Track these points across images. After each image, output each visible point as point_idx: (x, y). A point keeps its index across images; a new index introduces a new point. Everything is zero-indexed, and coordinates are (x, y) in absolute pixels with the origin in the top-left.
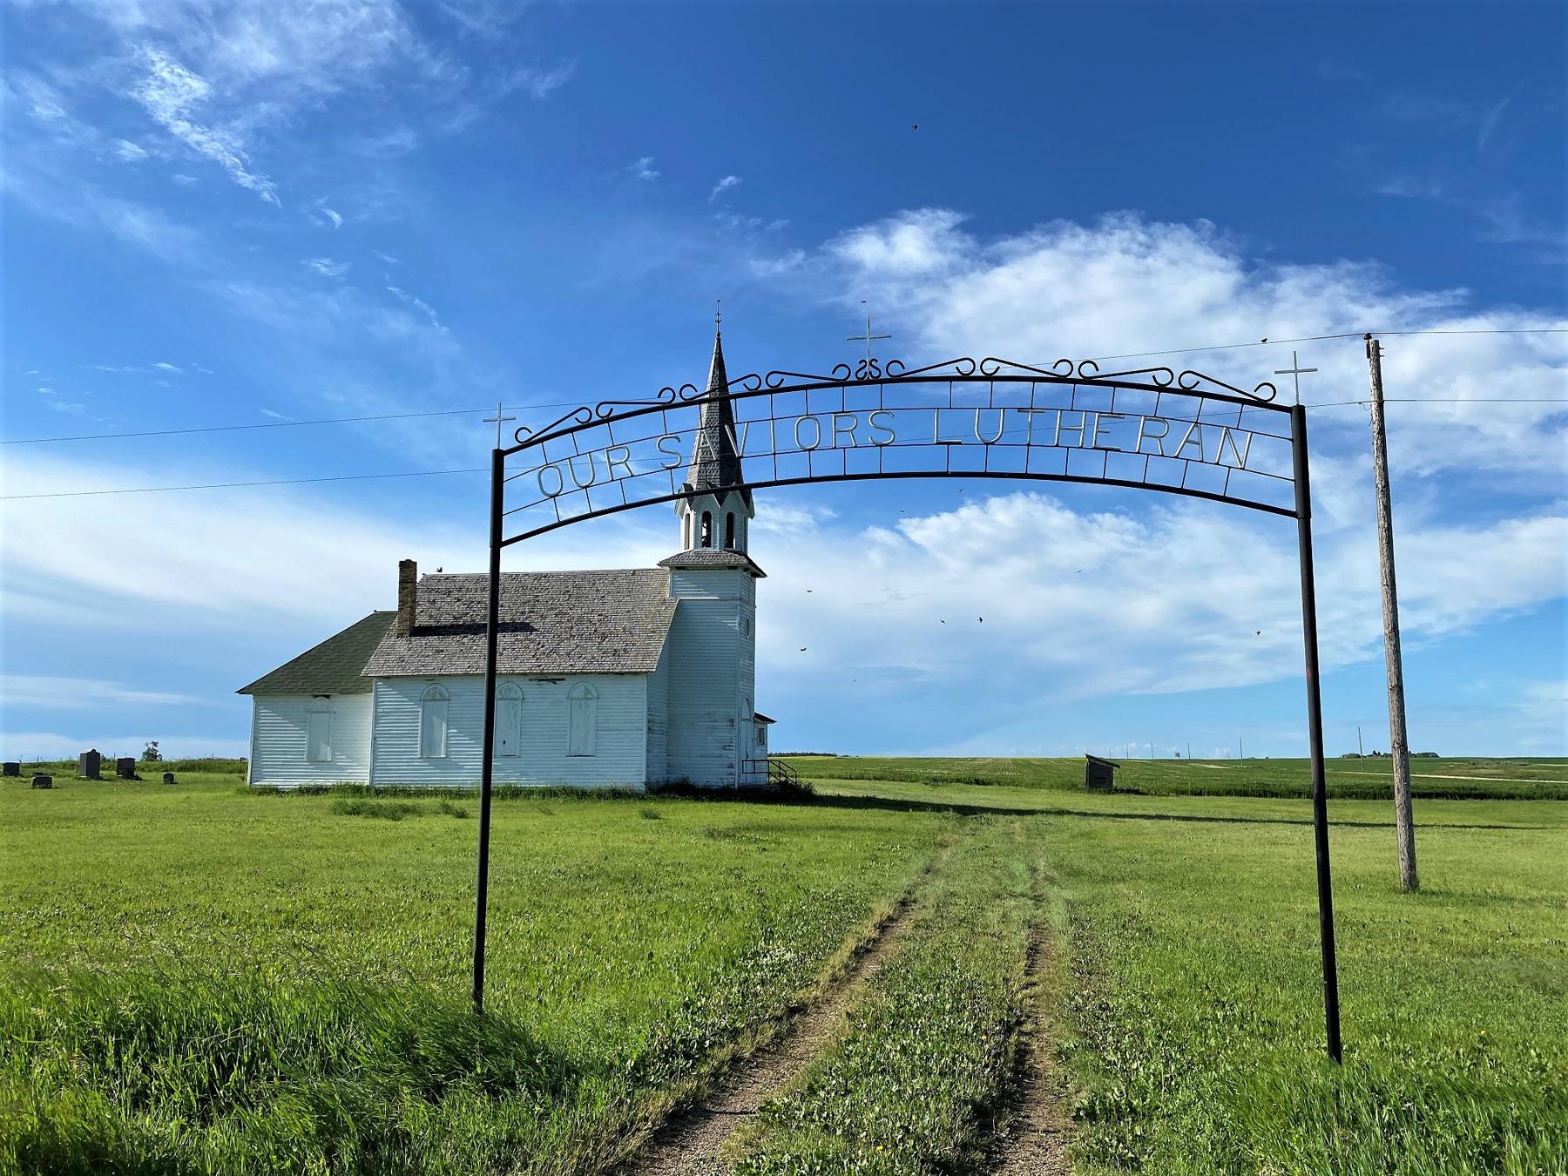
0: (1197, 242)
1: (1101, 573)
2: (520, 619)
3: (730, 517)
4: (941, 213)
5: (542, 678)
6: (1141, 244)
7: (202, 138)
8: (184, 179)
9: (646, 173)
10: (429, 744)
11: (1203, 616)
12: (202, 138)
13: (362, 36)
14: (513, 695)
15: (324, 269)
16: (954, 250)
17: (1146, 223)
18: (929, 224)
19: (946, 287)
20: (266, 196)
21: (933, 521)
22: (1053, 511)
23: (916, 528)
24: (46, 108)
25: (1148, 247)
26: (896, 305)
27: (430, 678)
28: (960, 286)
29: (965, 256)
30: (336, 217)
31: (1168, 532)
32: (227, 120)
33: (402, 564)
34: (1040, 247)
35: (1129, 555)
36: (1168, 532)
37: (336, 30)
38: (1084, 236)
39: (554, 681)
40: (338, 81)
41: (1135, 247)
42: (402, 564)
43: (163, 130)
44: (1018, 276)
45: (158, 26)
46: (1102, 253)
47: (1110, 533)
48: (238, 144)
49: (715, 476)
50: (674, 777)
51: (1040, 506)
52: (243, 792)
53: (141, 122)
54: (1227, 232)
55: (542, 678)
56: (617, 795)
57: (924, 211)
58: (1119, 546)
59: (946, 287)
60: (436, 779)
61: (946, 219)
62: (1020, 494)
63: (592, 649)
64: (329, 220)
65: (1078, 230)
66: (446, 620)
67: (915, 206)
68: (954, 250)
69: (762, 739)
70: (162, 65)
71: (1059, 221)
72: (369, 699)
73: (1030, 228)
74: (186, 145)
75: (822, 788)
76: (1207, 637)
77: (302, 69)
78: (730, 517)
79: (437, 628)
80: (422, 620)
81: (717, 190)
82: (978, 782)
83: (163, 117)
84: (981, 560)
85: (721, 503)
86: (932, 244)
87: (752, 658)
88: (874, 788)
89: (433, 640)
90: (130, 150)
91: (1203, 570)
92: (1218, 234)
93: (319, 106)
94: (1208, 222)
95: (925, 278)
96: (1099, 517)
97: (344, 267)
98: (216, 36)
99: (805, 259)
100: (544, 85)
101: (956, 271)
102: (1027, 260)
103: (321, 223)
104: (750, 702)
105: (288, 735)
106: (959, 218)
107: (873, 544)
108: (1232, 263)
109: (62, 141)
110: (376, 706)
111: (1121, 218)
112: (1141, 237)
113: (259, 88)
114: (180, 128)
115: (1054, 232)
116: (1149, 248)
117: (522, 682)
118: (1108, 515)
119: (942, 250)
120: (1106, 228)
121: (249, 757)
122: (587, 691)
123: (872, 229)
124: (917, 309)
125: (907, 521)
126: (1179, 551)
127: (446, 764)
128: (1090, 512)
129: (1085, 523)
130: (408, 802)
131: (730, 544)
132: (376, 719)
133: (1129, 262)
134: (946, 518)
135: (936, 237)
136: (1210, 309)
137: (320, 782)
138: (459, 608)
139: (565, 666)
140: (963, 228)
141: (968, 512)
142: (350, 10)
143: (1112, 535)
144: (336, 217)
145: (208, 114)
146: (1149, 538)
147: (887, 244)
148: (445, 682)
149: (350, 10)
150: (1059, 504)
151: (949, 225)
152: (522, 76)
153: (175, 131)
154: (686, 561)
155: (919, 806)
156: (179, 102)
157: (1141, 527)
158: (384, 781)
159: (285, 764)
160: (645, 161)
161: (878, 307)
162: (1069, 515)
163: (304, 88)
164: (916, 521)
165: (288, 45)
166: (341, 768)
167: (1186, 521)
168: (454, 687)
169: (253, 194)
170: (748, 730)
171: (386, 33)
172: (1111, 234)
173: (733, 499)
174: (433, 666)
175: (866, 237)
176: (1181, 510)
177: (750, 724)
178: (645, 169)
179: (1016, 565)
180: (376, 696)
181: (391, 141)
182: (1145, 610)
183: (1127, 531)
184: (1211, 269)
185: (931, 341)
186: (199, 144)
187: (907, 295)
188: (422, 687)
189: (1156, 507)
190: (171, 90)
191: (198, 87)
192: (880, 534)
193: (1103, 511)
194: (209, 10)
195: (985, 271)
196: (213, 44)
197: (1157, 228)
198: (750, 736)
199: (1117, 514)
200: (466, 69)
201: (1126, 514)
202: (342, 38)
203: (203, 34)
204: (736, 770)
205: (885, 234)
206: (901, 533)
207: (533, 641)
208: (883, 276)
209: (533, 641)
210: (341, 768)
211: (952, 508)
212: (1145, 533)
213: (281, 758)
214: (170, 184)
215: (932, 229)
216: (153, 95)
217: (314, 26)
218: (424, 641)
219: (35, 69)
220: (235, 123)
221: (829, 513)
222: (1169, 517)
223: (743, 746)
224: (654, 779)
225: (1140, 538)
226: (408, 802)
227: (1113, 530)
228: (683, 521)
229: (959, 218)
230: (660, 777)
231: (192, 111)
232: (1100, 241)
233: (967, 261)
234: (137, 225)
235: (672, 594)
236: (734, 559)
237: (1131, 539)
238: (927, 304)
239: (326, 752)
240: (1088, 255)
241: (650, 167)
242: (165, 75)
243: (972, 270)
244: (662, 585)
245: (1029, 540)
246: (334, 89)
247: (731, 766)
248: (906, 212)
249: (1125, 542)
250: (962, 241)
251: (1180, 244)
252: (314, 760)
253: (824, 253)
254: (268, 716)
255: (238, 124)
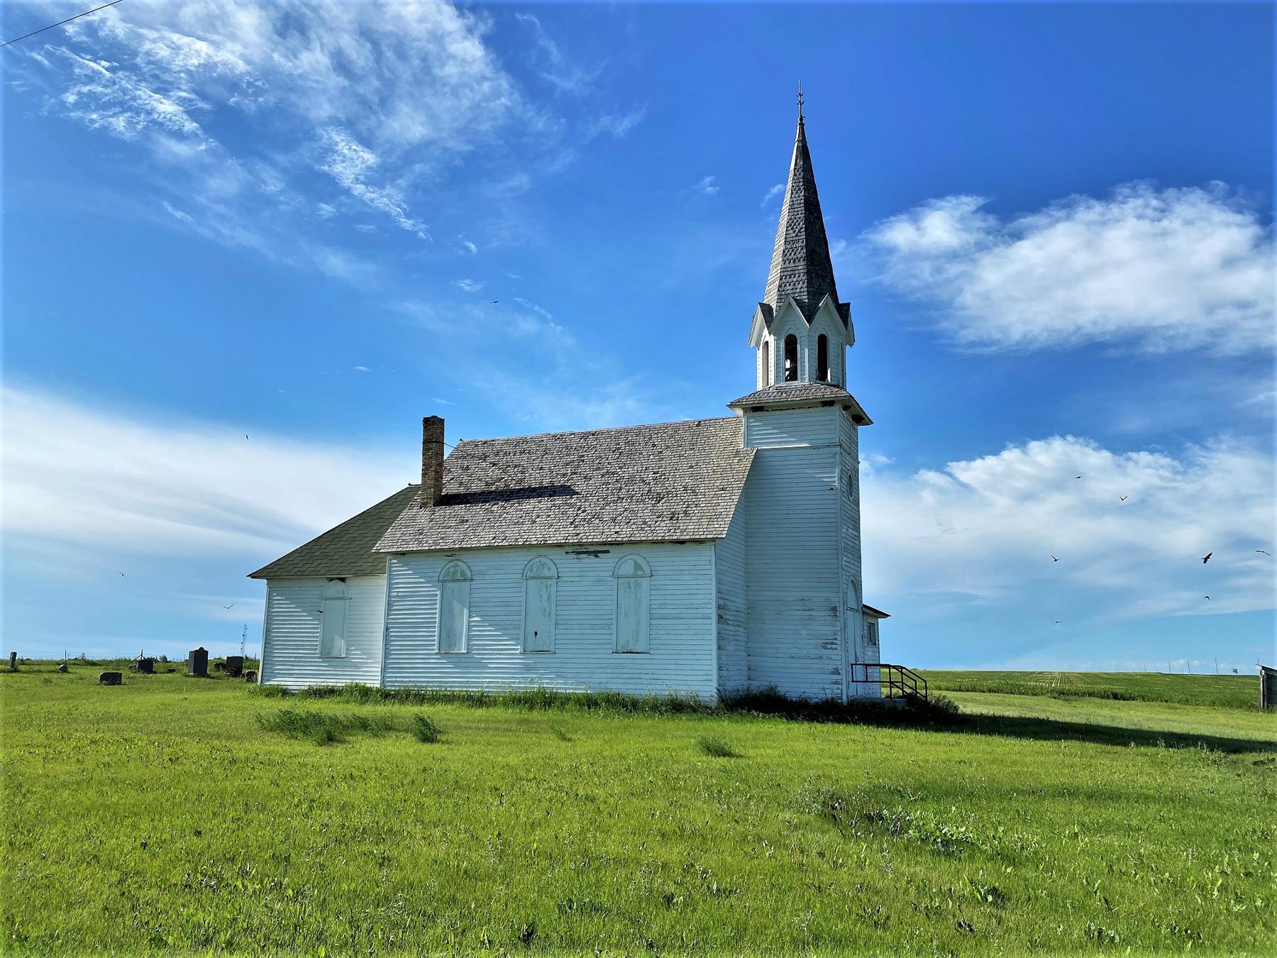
0: (1212, 202)
1: (1141, 506)
2: (560, 481)
3: (823, 341)
4: (964, 199)
5: (581, 549)
6: (1155, 209)
7: (373, 196)
8: (365, 228)
9: (710, 189)
10: (448, 637)
11: (1245, 543)
12: (373, 196)
13: (484, 104)
14: (546, 573)
15: (467, 288)
16: (978, 230)
17: (1158, 190)
18: (953, 208)
19: (973, 261)
20: (421, 234)
21: (978, 463)
22: (1089, 451)
23: (964, 470)
24: (273, 185)
25: (1163, 211)
26: (931, 280)
27: (451, 553)
28: (986, 260)
29: (989, 233)
30: (473, 247)
31: (1204, 467)
32: (393, 180)
33: (426, 421)
34: (1058, 220)
35: (1166, 488)
36: (1204, 467)
37: (466, 103)
38: (1098, 207)
39: (596, 554)
40: (470, 142)
41: (1149, 212)
42: (426, 421)
43: (347, 192)
44: (1040, 247)
45: (342, 116)
46: (1118, 221)
47: (1146, 471)
48: (400, 196)
49: (801, 290)
50: (759, 685)
51: (1077, 447)
52: (252, 693)
53: (328, 187)
54: (1241, 190)
55: (581, 549)
56: (677, 707)
57: (949, 198)
58: (1156, 481)
59: (973, 261)
60: (456, 681)
61: (969, 203)
62: (1058, 437)
63: (645, 511)
64: (468, 249)
65: (1093, 202)
66: (477, 487)
67: (941, 195)
68: (978, 230)
69: (872, 638)
70: (342, 142)
71: (1073, 196)
72: (382, 582)
73: (1047, 205)
74: (362, 202)
75: (970, 706)
76: (1250, 563)
77: (444, 135)
78: (823, 341)
79: (466, 495)
80: (450, 488)
81: (767, 197)
82: (1116, 697)
83: (347, 181)
84: (1027, 497)
85: (809, 320)
86: (958, 225)
87: (857, 529)
88: (1002, 703)
89: (460, 509)
90: (326, 209)
91: (1241, 501)
92: (1231, 193)
93: (458, 162)
94: (1221, 183)
95: (953, 255)
96: (1134, 455)
97: (479, 287)
98: (383, 118)
99: (847, 248)
100: (623, 126)
101: (981, 247)
102: (1046, 232)
103: (461, 252)
104: (857, 585)
105: (303, 627)
106: (981, 201)
107: (925, 485)
108: (1248, 218)
109: (284, 207)
110: (390, 587)
111: (1134, 188)
112: (1155, 203)
113: (416, 152)
114: (359, 189)
115: (1070, 207)
116: (1163, 211)
117: (559, 556)
118: (1142, 454)
119: (967, 229)
120: (1120, 198)
121: (260, 657)
122: (637, 566)
123: (903, 217)
124: (949, 281)
125: (954, 464)
126: (1215, 483)
127: (466, 662)
128: (1125, 451)
129: (1121, 460)
130: (368, 710)
131: (822, 376)
132: (390, 604)
133: (1145, 226)
134: (990, 460)
135: (962, 219)
136: (1230, 262)
137: (331, 683)
138: (494, 473)
139: (609, 534)
140: (985, 210)
141: (1011, 455)
142: (476, 86)
143: (1148, 471)
144: (473, 247)
145: (376, 178)
146: (1184, 473)
147: (918, 229)
148: (466, 557)
149: (476, 86)
150: (1096, 445)
151: (972, 207)
152: (605, 121)
153: (355, 193)
154: (764, 399)
155: (1144, 738)
156: (357, 170)
157: (1176, 463)
158: (399, 681)
159: (298, 661)
160: (708, 180)
161: (914, 282)
162: (1106, 455)
163: (446, 150)
164: (963, 464)
165: (433, 118)
166: (356, 666)
167: (1221, 456)
168: (477, 563)
169: (413, 234)
170: (855, 624)
171: (503, 100)
172: (1124, 203)
173: (826, 321)
174: (452, 539)
175: (898, 225)
176: (1215, 446)
177: (858, 616)
178: (708, 186)
179: (1059, 500)
180: (390, 578)
181: (512, 183)
182: (1186, 539)
183: (1162, 467)
184: (1228, 225)
185: (963, 308)
186: (372, 200)
187: (938, 270)
188: (439, 564)
189: (1189, 445)
190: (351, 161)
191: (369, 158)
192: (931, 476)
193: (1138, 450)
194: (376, 99)
195: (1008, 245)
196: (380, 124)
197: (1171, 193)
198: (859, 632)
199: (1152, 452)
200: (563, 120)
201: (1159, 451)
202: (471, 108)
203: (373, 118)
204: (843, 678)
205: (915, 220)
206: (950, 475)
207: (571, 506)
208: (915, 256)
209: (571, 506)
210: (356, 666)
211: (996, 452)
212: (1181, 468)
213: (294, 653)
214: (356, 230)
215: (958, 213)
216: (338, 168)
217: (449, 102)
218: (448, 510)
219: (263, 157)
220: (400, 181)
221: (882, 459)
222: (1203, 453)
223: (851, 645)
224: (730, 686)
225: (1176, 473)
226: (368, 710)
227: (1148, 466)
228: (760, 353)
229: (981, 201)
230: (738, 683)
231: (366, 177)
232: (1115, 210)
233: (991, 238)
234: (336, 263)
235: (747, 444)
236: (829, 393)
237: (1166, 473)
238: (957, 277)
239: (340, 646)
240: (1103, 224)
241: (711, 185)
242: (345, 151)
243: (996, 245)
244: (735, 434)
245: (1071, 478)
246: (468, 148)
247: (836, 672)
248: (933, 201)
249: (1161, 477)
250: (985, 221)
251: (1193, 205)
252: (328, 656)
253: (862, 241)
254: (282, 605)
255: (401, 182)
